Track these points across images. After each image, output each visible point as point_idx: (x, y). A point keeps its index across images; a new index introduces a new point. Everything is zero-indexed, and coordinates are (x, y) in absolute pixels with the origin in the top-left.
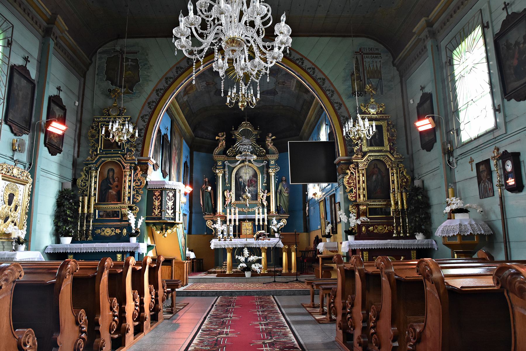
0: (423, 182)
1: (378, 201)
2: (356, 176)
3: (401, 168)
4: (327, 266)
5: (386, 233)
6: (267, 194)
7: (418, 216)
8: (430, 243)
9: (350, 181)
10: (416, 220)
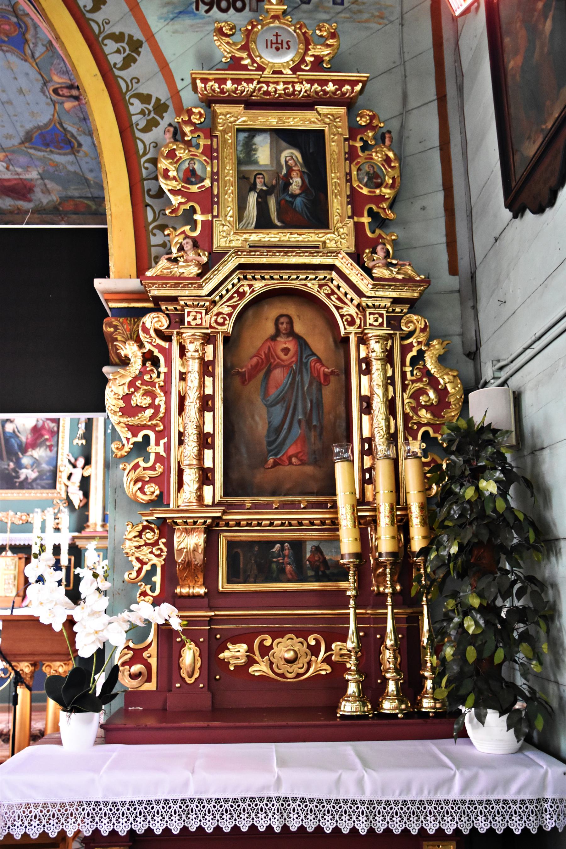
0: (517, 398)
1: (283, 505)
2: (168, 375)
3: (411, 334)
4: (224, 722)
5: (317, 677)
6: (83, 468)
7: (475, 602)
8: (549, 795)
9: (138, 399)
10: (465, 631)
